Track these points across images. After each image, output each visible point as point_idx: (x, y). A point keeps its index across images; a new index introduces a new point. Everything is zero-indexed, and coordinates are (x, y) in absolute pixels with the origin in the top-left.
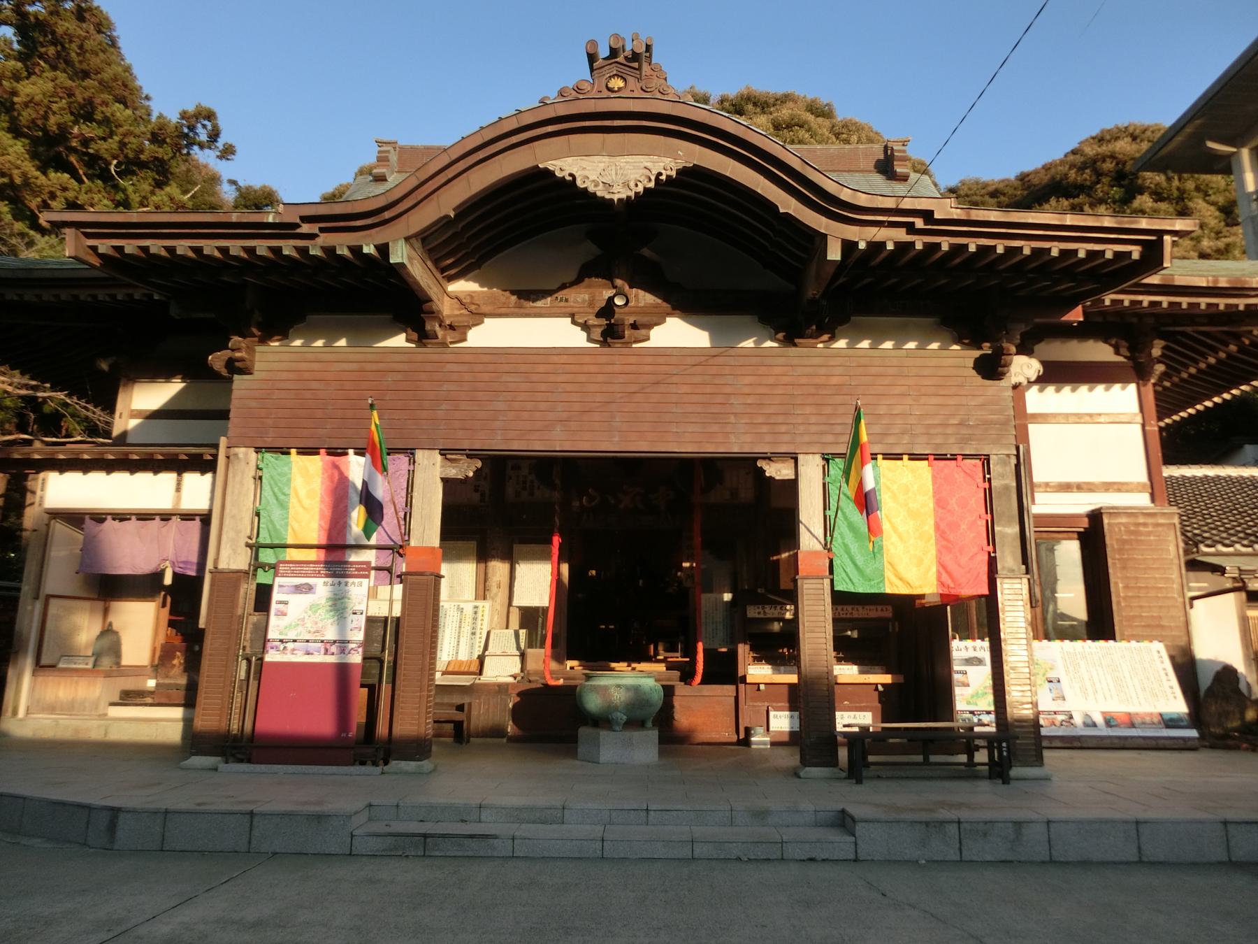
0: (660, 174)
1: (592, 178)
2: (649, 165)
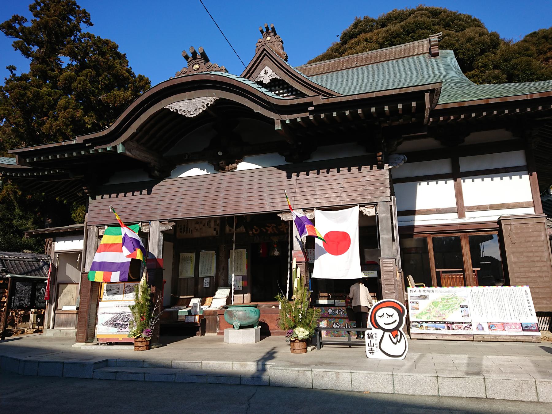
0: (208, 104)
1: (183, 109)
2: (204, 101)
